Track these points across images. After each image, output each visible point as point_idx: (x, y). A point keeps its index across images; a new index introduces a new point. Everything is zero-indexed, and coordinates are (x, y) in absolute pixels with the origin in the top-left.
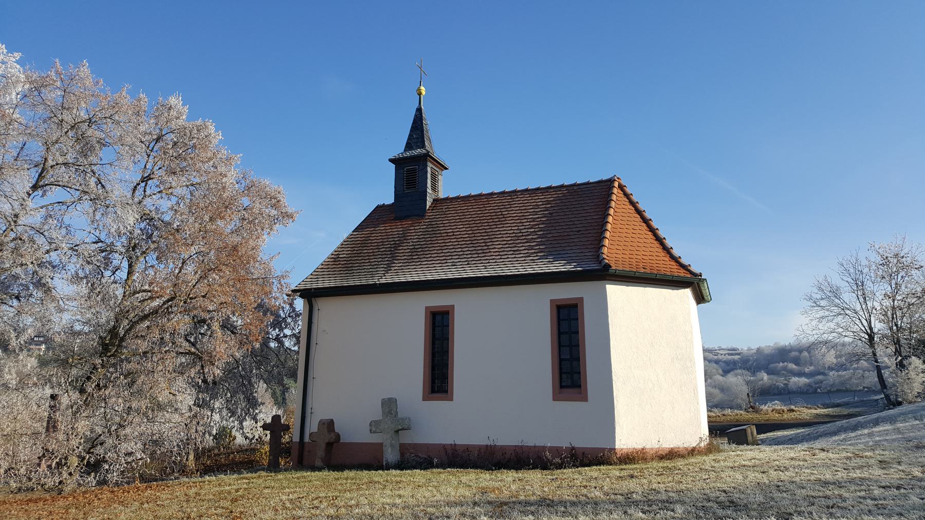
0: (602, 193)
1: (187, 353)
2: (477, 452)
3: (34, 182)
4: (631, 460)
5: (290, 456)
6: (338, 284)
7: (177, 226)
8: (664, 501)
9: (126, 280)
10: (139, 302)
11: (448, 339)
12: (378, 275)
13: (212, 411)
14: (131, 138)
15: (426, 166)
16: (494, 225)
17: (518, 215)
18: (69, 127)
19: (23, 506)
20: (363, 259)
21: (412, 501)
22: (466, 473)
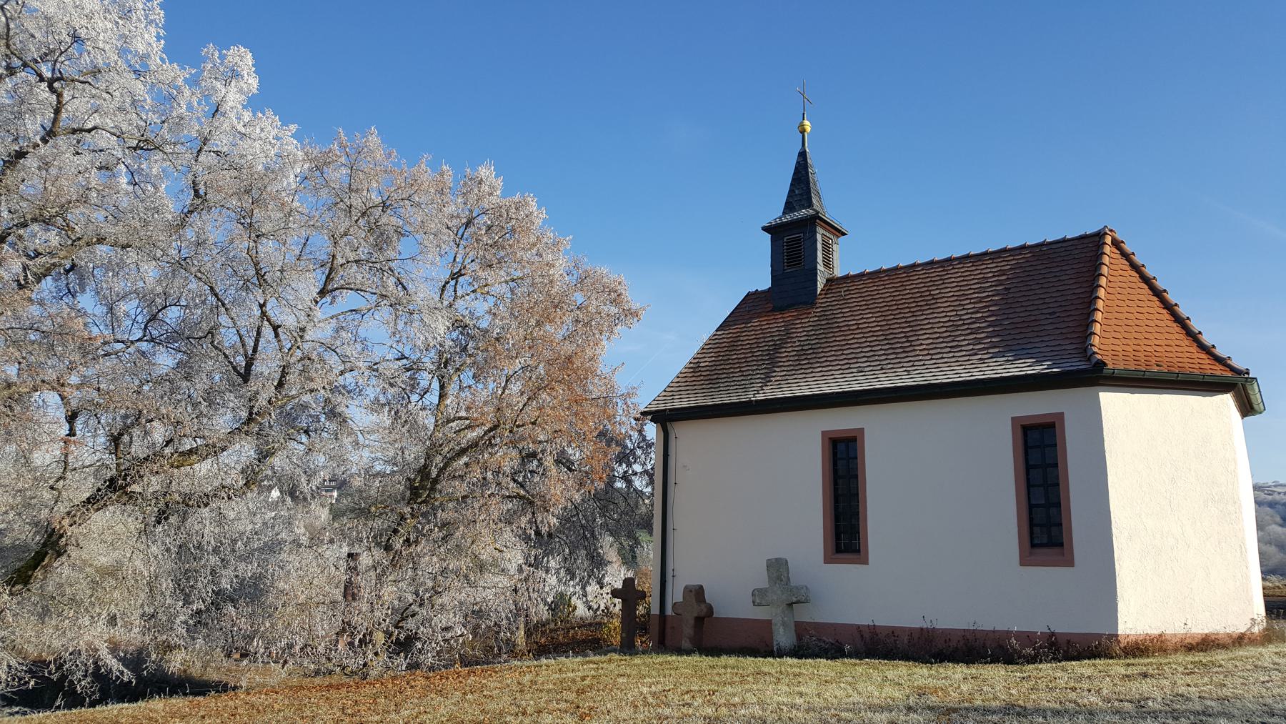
0: (1088, 254)
1: (515, 497)
2: (906, 637)
3: (321, 287)
4: (1142, 652)
5: (646, 633)
6: (701, 402)
7: (497, 333)
8: (1198, 712)
9: (438, 405)
10: (455, 432)
11: (856, 477)
12: (753, 389)
13: (547, 572)
14: (436, 224)
15: (815, 232)
16: (920, 310)
17: (956, 294)
18: (359, 214)
19: (323, 693)
20: (731, 368)
21: (818, 702)
22: (893, 666)
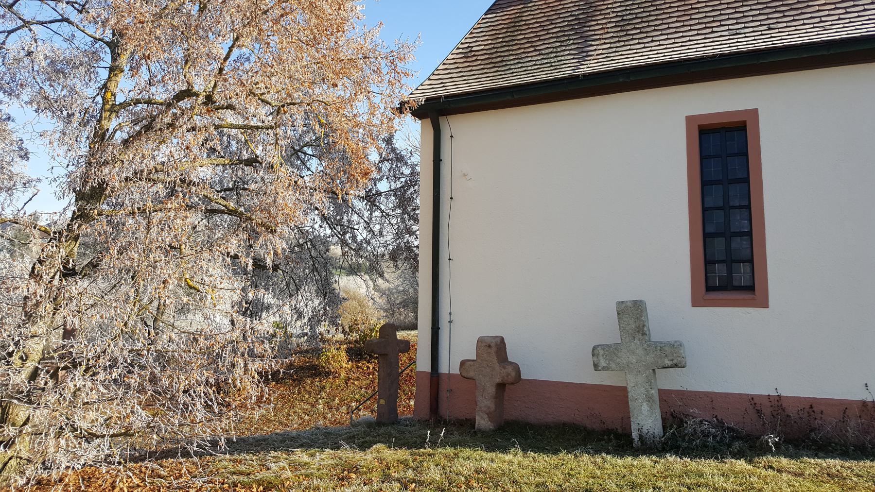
6: (488, 84)
